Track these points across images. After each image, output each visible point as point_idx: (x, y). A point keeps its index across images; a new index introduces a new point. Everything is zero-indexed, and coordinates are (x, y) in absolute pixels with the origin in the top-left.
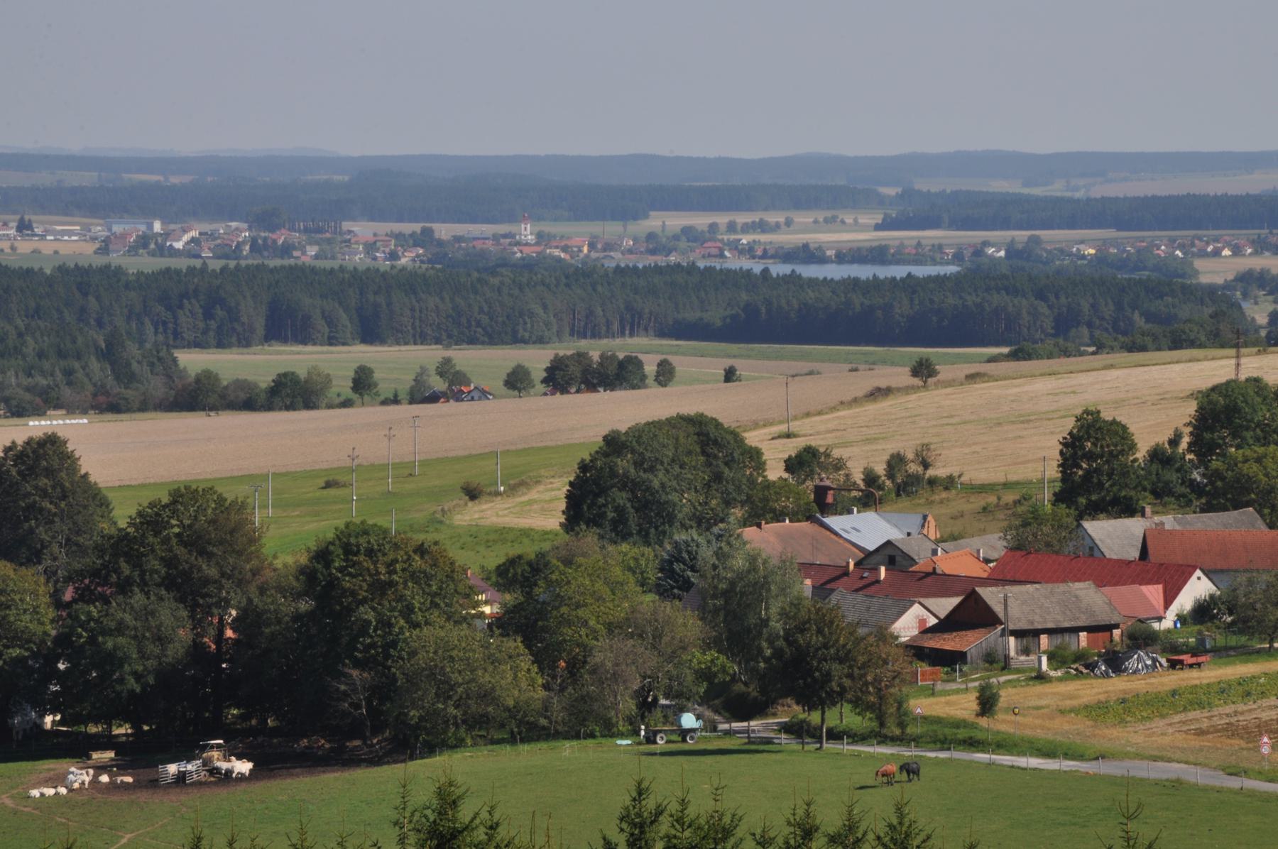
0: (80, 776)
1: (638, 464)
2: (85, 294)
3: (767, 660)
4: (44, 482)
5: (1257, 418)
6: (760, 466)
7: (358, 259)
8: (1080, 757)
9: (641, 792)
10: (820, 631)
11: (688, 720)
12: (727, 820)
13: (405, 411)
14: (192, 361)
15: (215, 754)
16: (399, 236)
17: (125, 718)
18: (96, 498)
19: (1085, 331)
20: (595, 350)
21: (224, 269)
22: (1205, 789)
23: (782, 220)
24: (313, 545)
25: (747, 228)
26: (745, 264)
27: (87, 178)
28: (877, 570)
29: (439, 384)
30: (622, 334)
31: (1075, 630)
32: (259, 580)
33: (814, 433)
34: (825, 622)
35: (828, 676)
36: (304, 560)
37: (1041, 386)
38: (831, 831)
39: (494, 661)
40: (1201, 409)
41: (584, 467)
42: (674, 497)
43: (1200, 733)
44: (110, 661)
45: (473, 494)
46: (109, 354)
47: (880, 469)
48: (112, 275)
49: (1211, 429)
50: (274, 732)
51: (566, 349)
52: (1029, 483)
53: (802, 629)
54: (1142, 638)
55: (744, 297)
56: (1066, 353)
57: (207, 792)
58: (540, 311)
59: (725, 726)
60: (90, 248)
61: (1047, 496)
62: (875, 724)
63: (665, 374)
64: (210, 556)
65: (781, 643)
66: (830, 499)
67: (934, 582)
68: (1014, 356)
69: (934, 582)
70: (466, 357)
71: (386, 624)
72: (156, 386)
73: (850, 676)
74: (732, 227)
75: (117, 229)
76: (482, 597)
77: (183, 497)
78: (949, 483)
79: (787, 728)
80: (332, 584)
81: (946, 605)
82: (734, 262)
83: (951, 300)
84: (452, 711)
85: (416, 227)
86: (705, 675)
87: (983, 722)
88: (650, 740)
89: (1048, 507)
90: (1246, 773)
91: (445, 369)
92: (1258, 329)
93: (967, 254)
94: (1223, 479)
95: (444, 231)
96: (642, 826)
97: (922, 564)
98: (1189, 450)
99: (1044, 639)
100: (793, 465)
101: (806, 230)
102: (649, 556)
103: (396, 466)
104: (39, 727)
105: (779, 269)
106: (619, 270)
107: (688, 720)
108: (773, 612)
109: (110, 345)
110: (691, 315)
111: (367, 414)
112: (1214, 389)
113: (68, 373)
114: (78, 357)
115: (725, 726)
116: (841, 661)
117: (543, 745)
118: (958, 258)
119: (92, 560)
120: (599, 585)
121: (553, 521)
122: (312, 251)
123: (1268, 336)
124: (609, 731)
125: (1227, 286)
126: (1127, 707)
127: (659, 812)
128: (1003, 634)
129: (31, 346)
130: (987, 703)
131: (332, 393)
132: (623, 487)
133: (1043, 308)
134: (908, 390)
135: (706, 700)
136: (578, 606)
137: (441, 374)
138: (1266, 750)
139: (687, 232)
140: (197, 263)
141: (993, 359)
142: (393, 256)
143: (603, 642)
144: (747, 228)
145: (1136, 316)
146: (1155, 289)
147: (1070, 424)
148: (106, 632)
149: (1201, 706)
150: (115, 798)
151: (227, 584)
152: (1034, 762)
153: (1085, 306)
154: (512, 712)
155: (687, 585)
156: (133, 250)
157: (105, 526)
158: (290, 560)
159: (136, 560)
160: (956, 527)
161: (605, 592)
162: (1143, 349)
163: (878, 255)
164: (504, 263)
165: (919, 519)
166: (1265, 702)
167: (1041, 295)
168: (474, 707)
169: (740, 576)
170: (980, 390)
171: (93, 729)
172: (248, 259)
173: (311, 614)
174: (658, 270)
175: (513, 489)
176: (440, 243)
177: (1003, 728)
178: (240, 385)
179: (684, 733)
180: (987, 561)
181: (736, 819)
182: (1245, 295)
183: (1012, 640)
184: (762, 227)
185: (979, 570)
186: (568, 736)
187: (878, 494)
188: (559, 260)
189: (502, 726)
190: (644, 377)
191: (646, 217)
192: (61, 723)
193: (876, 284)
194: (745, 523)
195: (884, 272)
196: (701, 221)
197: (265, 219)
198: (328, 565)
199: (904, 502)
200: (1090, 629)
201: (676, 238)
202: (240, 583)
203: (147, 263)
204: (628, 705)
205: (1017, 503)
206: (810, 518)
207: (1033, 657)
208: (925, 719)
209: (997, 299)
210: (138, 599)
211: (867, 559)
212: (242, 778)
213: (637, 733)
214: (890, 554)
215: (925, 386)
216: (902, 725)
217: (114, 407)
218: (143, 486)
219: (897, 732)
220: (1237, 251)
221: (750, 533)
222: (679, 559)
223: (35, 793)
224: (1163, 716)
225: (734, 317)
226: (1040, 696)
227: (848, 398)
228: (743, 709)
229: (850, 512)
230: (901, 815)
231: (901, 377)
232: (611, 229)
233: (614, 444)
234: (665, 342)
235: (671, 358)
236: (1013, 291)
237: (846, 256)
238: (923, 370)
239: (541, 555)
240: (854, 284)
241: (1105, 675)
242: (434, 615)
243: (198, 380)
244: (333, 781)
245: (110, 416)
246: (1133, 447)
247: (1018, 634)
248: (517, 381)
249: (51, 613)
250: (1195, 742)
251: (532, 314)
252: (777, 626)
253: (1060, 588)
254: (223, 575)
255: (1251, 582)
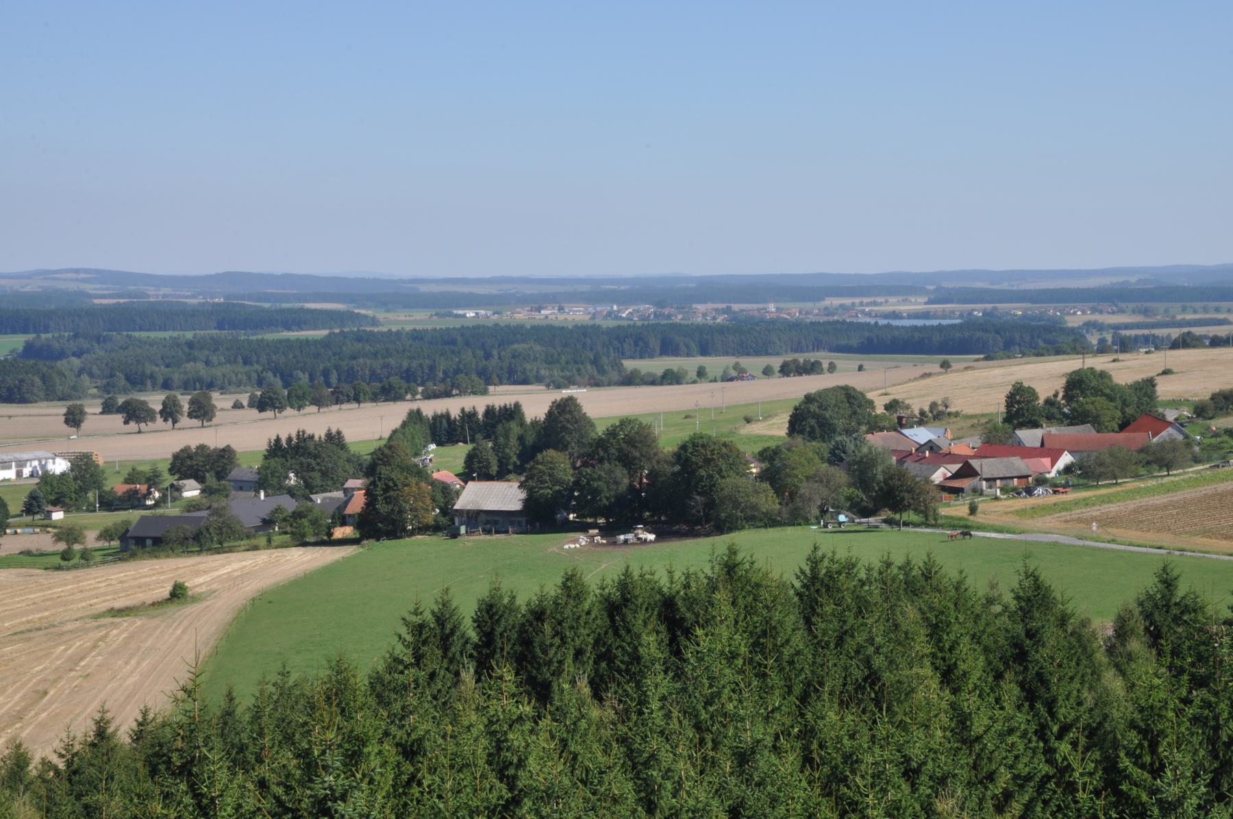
0: (583, 539)
1: (820, 407)
2: (585, 337)
3: (876, 492)
4: (568, 416)
5: (1092, 385)
6: (873, 408)
7: (699, 320)
8: (1014, 533)
9: (816, 548)
10: (899, 479)
11: (842, 518)
12: (854, 560)
13: (719, 385)
14: (629, 364)
15: (640, 531)
16: (716, 310)
17: (603, 516)
18: (590, 424)
19: (1017, 348)
20: (801, 358)
21: (643, 325)
22: (1068, 546)
23: (883, 300)
24: (680, 443)
25: (868, 304)
26: (867, 320)
27: (586, 288)
28: (924, 452)
29: (733, 373)
30: (813, 350)
31: (1012, 478)
32: (657, 458)
33: (897, 393)
34: (902, 475)
35: (903, 499)
36: (676, 449)
37: (997, 372)
38: (900, 565)
39: (757, 492)
40: (1068, 382)
41: (796, 409)
42: (836, 421)
43: (1066, 521)
44: (596, 492)
45: (748, 420)
46: (595, 362)
47: (927, 409)
48: (596, 328)
49: (1071, 390)
50: (664, 523)
51: (789, 357)
52: (991, 414)
53: (891, 478)
54: (1041, 481)
55: (867, 334)
56: (1009, 358)
57: (637, 547)
58: (777, 341)
59: (857, 520)
60: (587, 317)
61: (1000, 420)
62: (924, 519)
63: (832, 368)
64: (636, 447)
65: (882, 484)
66: (904, 422)
67: (949, 457)
68: (986, 359)
69: (949, 457)
70: (745, 361)
71: (711, 477)
72: (615, 376)
73: (913, 499)
74: (861, 304)
75: (599, 309)
76: (752, 465)
77: (624, 422)
78: (957, 414)
79: (885, 521)
80: (687, 460)
81: (955, 467)
82: (862, 319)
83: (958, 335)
84: (739, 514)
85: (724, 306)
86: (849, 498)
87: (971, 518)
88: (825, 526)
89: (1000, 424)
90: (1086, 538)
91: (736, 367)
92: (1092, 347)
93: (965, 315)
94: (1077, 411)
95: (736, 307)
96: (816, 562)
97: (945, 450)
98: (1063, 399)
99: (998, 482)
100: (889, 407)
101: (894, 304)
102: (825, 447)
103: (715, 409)
104: (567, 519)
105: (882, 322)
106: (812, 323)
107: (842, 518)
108: (879, 472)
109: (595, 358)
110: (843, 342)
111: (703, 386)
112: (1074, 372)
113: (578, 370)
114: (582, 363)
115: (857, 520)
116: (909, 492)
117: (779, 529)
118: (961, 316)
119: (587, 450)
120: (802, 460)
121: (782, 431)
122: (680, 317)
123: (1098, 350)
124: (807, 522)
125: (1079, 328)
126: (1035, 511)
127: (824, 557)
128: (980, 480)
129: (563, 359)
130: (973, 510)
131: (689, 377)
132: (813, 417)
133: (999, 338)
134: (939, 374)
135: (850, 509)
136: (793, 469)
137: (735, 368)
138: (1094, 528)
139: (842, 306)
140: (632, 323)
141: (977, 360)
142: (714, 318)
143: (805, 484)
144: (868, 304)
145: (1040, 341)
146: (1047, 329)
147: (1010, 388)
148: (594, 480)
149: (1067, 510)
150: (599, 549)
151: (643, 459)
152: (994, 535)
153: (1017, 336)
154: (766, 514)
155: (841, 460)
156: (605, 317)
157: (593, 435)
158: (670, 449)
159: (606, 450)
160: (960, 434)
161: (805, 463)
162: (1042, 355)
163: (926, 315)
164: (762, 321)
165: (943, 430)
166: (1095, 508)
167: (997, 332)
168: (749, 513)
169: (866, 456)
170: (970, 375)
171: (589, 520)
172: (653, 320)
173: (679, 473)
174: (829, 323)
175: (765, 419)
176: (735, 313)
177: (980, 520)
178: (649, 374)
179: (840, 524)
180: (973, 448)
181: (858, 560)
182: (1087, 332)
183: (984, 483)
184: (875, 304)
185: (970, 452)
186: (790, 525)
187: (925, 419)
188: (786, 319)
189: (761, 520)
190: (822, 370)
191: (824, 300)
192: (577, 517)
193: (925, 328)
194: (867, 432)
195: (928, 323)
196: (847, 301)
197: (660, 304)
198: (686, 451)
199: (937, 423)
200: (1019, 477)
201: (837, 309)
202: (649, 459)
203: (611, 323)
204: (815, 512)
205: (987, 423)
206: (895, 430)
207: (993, 490)
208: (946, 517)
209: (978, 334)
210: (606, 465)
211: (921, 448)
212: (651, 541)
213: (819, 523)
214: (931, 446)
215: (946, 373)
216: (935, 519)
217: (597, 384)
218: (609, 418)
219: (933, 522)
220: (1084, 312)
221: (869, 437)
222: (838, 449)
223: (566, 547)
224: (1050, 515)
225: (862, 343)
226: (996, 506)
227: (912, 377)
228: (866, 513)
229: (912, 427)
230: (929, 559)
231: (936, 368)
232: (809, 305)
233: (809, 399)
234: (833, 354)
235: (834, 361)
236: (986, 331)
237: (917, 316)
238: (945, 365)
239: (778, 447)
240: (915, 328)
241: (1025, 497)
242: (731, 473)
243: (632, 373)
244: (689, 543)
245: (595, 388)
246: (1037, 398)
247: (987, 480)
248: (767, 372)
249: (572, 471)
250: (1064, 526)
251: (774, 343)
252: (880, 477)
253: (1006, 459)
254: (642, 455)
255: (1089, 456)
